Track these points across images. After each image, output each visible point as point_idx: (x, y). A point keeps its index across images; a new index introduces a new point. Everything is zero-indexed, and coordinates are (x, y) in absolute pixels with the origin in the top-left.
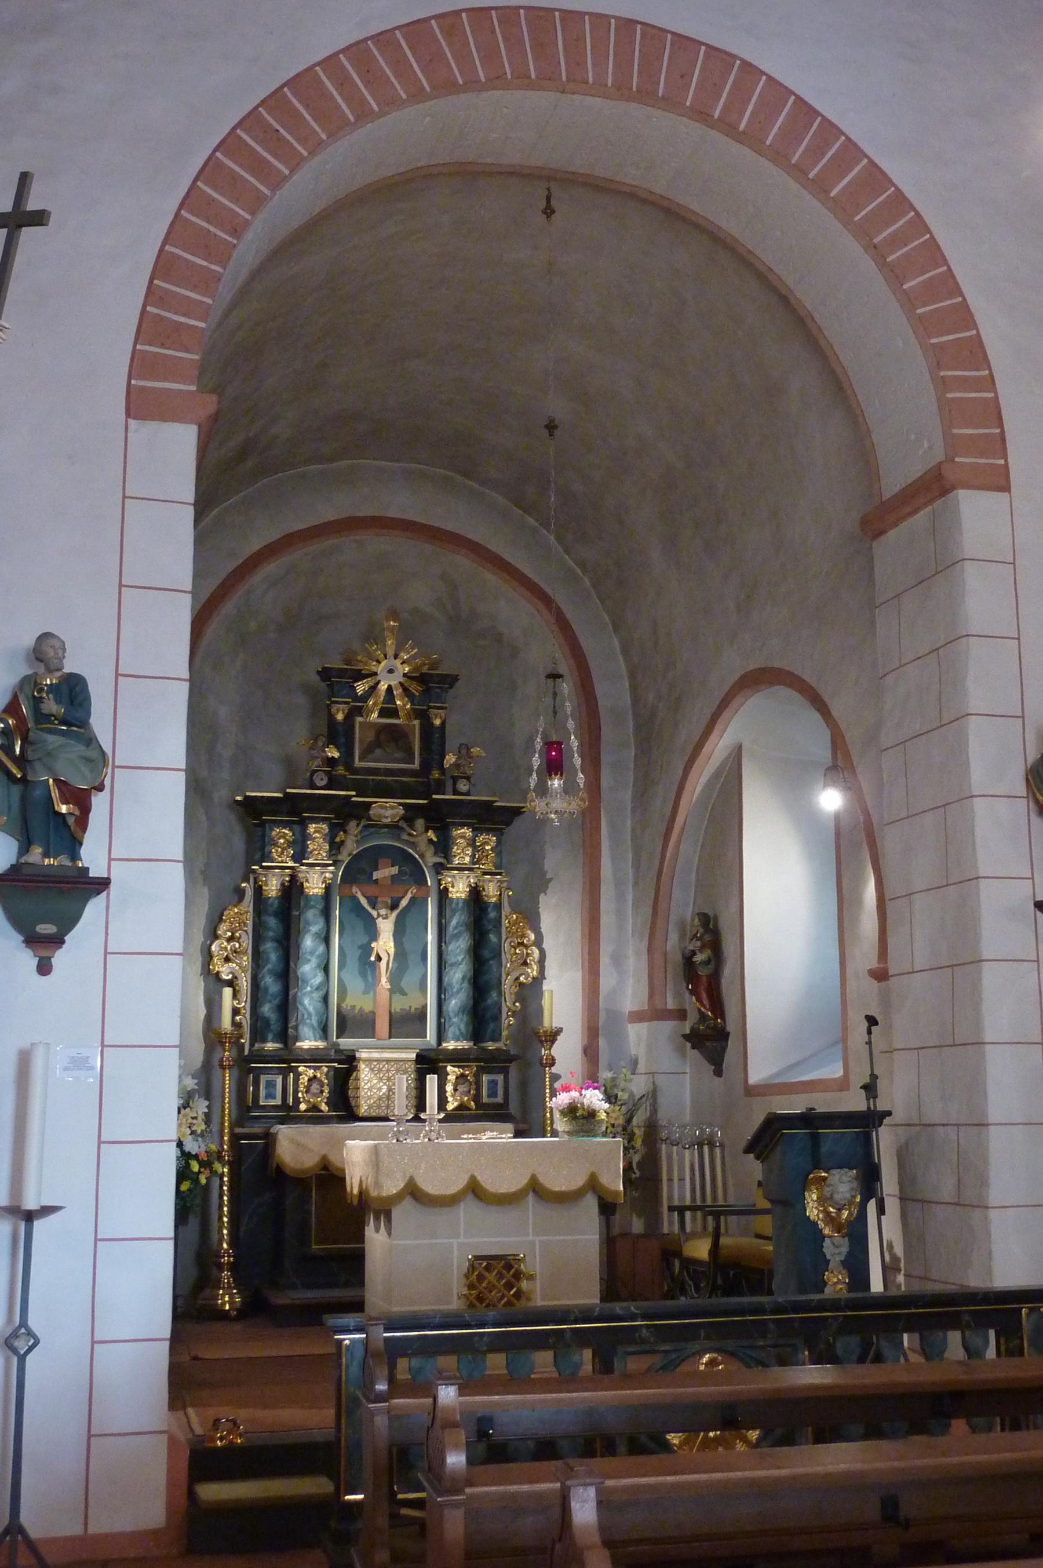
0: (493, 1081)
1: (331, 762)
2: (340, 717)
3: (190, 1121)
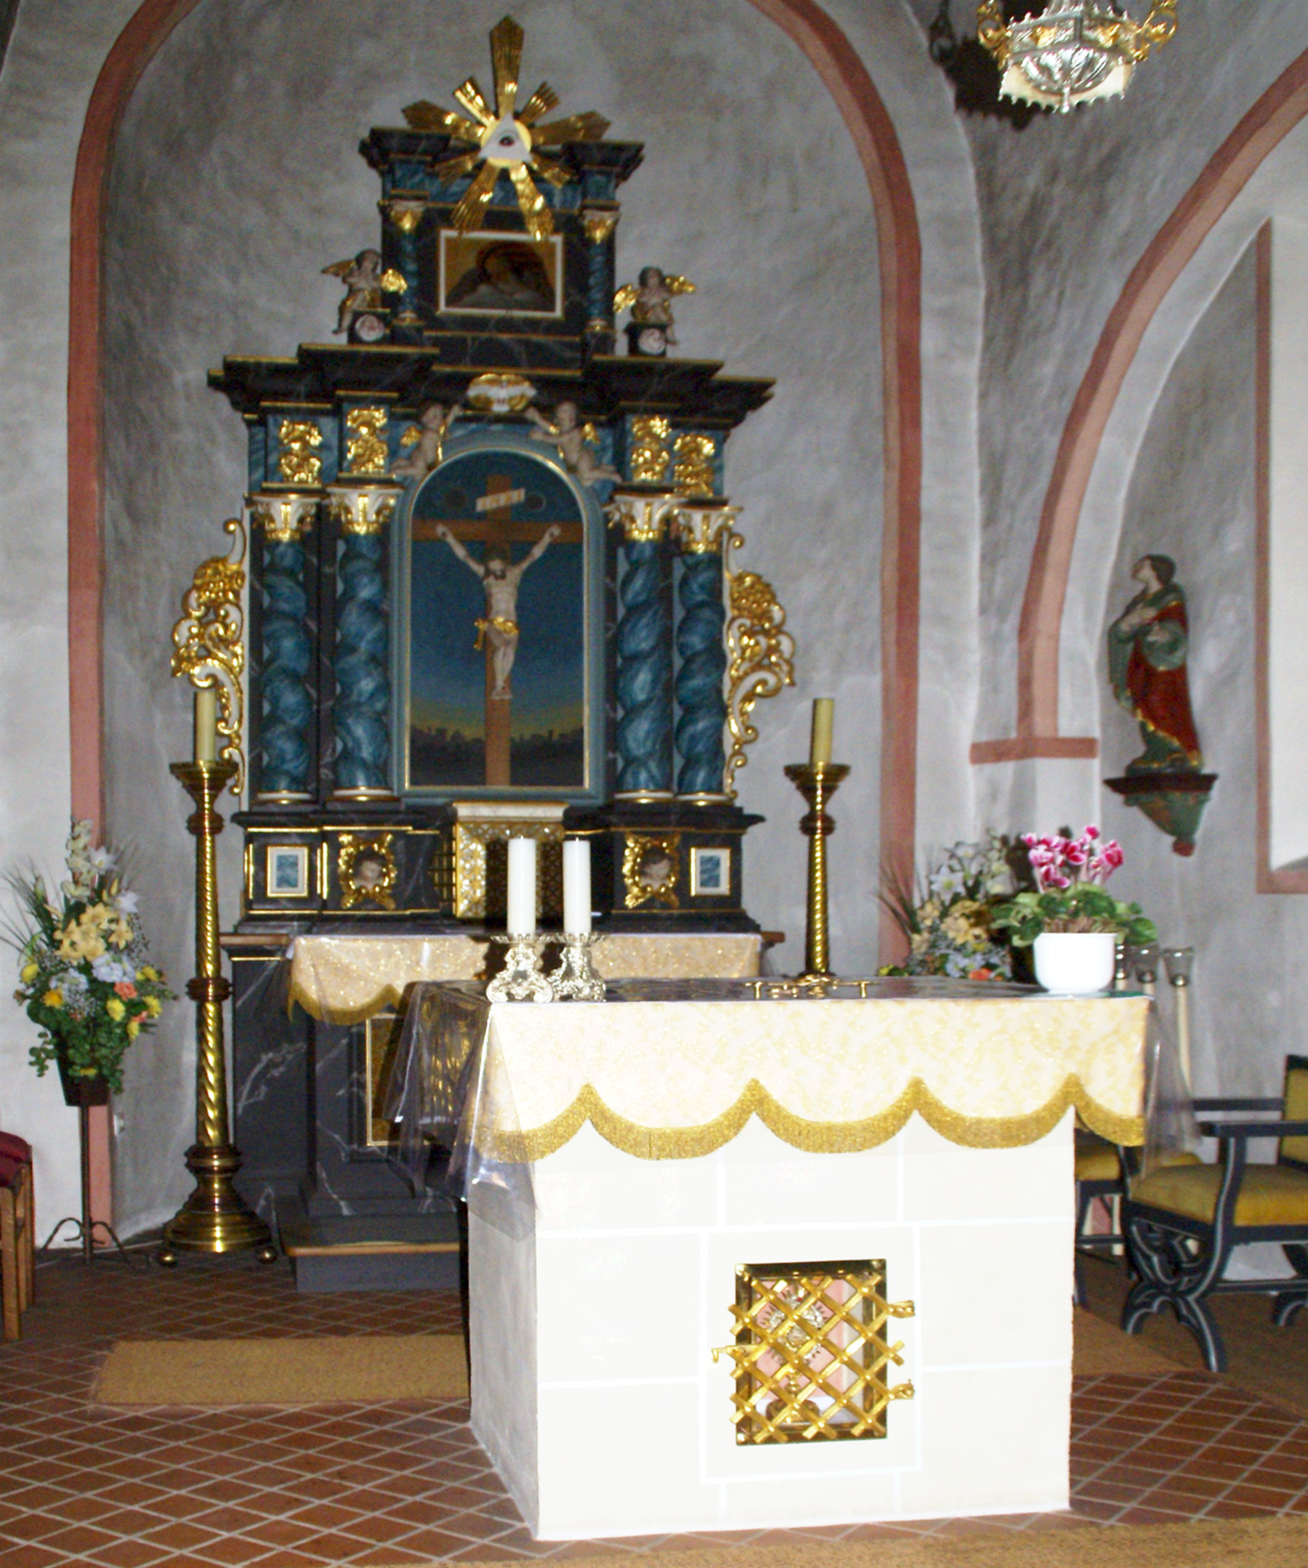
0: (710, 859)
1: (391, 300)
2: (407, 225)
3: (105, 925)
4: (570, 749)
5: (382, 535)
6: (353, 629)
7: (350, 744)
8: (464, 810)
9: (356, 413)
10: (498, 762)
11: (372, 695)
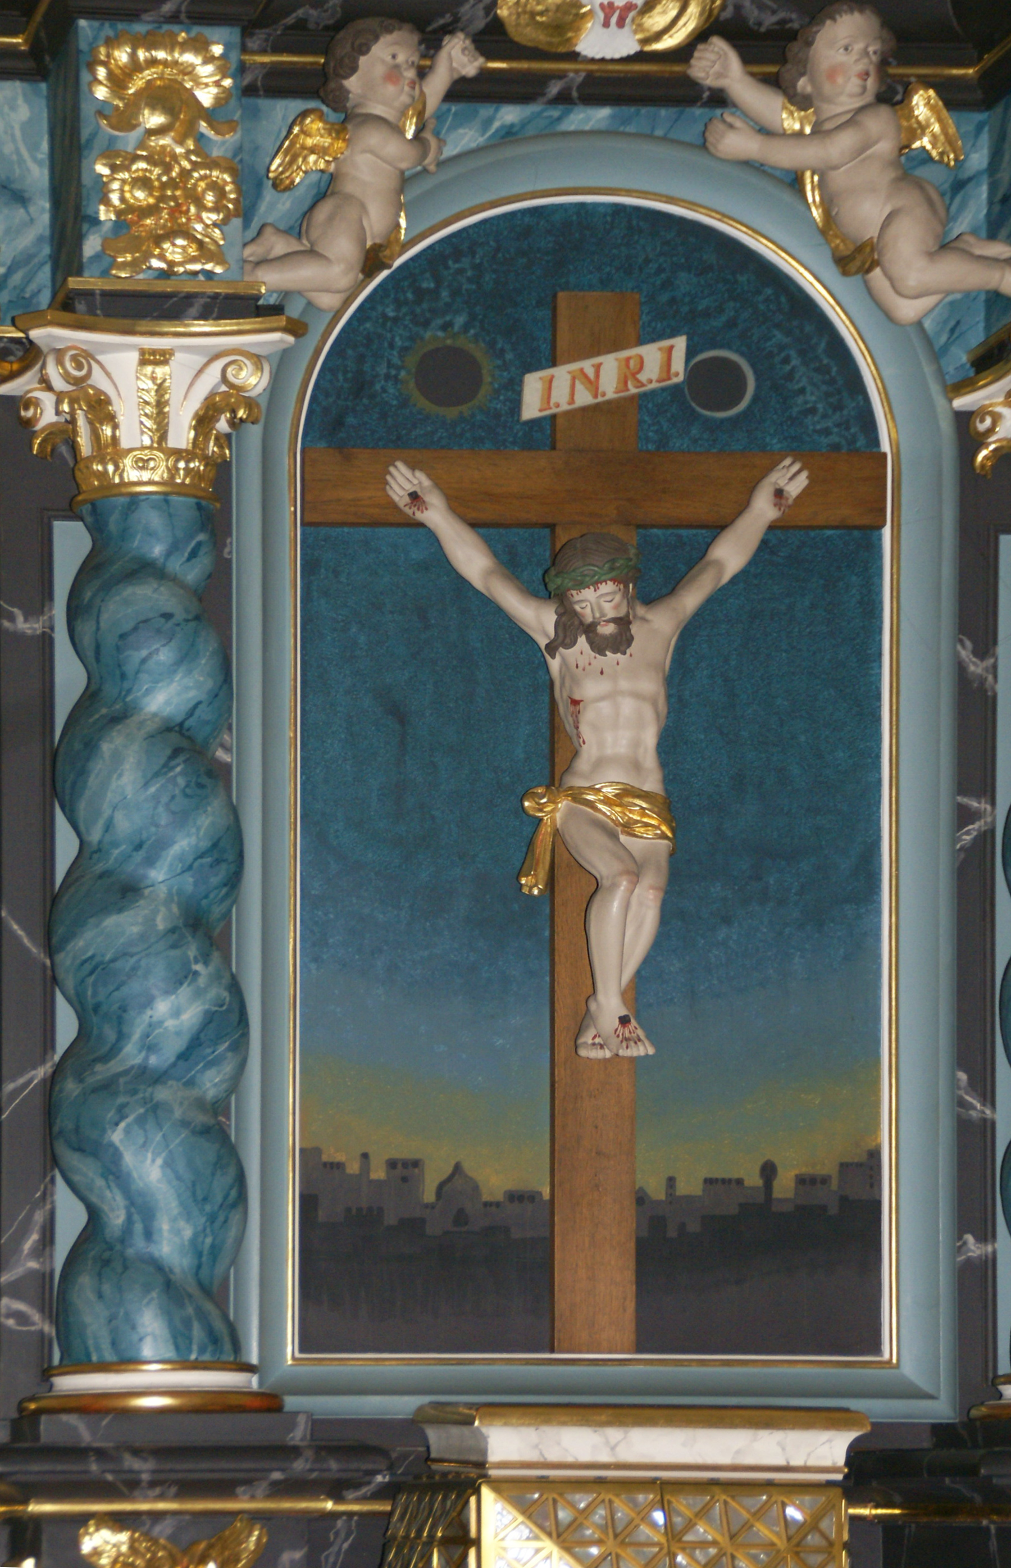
4: (840, 1223)
5: (209, 504)
6: (124, 825)
7: (116, 1218)
8: (506, 1443)
9: (122, 56)
10: (597, 1275)
11: (194, 1048)
